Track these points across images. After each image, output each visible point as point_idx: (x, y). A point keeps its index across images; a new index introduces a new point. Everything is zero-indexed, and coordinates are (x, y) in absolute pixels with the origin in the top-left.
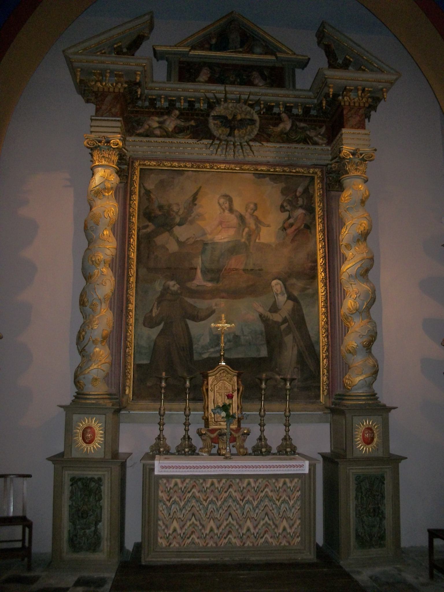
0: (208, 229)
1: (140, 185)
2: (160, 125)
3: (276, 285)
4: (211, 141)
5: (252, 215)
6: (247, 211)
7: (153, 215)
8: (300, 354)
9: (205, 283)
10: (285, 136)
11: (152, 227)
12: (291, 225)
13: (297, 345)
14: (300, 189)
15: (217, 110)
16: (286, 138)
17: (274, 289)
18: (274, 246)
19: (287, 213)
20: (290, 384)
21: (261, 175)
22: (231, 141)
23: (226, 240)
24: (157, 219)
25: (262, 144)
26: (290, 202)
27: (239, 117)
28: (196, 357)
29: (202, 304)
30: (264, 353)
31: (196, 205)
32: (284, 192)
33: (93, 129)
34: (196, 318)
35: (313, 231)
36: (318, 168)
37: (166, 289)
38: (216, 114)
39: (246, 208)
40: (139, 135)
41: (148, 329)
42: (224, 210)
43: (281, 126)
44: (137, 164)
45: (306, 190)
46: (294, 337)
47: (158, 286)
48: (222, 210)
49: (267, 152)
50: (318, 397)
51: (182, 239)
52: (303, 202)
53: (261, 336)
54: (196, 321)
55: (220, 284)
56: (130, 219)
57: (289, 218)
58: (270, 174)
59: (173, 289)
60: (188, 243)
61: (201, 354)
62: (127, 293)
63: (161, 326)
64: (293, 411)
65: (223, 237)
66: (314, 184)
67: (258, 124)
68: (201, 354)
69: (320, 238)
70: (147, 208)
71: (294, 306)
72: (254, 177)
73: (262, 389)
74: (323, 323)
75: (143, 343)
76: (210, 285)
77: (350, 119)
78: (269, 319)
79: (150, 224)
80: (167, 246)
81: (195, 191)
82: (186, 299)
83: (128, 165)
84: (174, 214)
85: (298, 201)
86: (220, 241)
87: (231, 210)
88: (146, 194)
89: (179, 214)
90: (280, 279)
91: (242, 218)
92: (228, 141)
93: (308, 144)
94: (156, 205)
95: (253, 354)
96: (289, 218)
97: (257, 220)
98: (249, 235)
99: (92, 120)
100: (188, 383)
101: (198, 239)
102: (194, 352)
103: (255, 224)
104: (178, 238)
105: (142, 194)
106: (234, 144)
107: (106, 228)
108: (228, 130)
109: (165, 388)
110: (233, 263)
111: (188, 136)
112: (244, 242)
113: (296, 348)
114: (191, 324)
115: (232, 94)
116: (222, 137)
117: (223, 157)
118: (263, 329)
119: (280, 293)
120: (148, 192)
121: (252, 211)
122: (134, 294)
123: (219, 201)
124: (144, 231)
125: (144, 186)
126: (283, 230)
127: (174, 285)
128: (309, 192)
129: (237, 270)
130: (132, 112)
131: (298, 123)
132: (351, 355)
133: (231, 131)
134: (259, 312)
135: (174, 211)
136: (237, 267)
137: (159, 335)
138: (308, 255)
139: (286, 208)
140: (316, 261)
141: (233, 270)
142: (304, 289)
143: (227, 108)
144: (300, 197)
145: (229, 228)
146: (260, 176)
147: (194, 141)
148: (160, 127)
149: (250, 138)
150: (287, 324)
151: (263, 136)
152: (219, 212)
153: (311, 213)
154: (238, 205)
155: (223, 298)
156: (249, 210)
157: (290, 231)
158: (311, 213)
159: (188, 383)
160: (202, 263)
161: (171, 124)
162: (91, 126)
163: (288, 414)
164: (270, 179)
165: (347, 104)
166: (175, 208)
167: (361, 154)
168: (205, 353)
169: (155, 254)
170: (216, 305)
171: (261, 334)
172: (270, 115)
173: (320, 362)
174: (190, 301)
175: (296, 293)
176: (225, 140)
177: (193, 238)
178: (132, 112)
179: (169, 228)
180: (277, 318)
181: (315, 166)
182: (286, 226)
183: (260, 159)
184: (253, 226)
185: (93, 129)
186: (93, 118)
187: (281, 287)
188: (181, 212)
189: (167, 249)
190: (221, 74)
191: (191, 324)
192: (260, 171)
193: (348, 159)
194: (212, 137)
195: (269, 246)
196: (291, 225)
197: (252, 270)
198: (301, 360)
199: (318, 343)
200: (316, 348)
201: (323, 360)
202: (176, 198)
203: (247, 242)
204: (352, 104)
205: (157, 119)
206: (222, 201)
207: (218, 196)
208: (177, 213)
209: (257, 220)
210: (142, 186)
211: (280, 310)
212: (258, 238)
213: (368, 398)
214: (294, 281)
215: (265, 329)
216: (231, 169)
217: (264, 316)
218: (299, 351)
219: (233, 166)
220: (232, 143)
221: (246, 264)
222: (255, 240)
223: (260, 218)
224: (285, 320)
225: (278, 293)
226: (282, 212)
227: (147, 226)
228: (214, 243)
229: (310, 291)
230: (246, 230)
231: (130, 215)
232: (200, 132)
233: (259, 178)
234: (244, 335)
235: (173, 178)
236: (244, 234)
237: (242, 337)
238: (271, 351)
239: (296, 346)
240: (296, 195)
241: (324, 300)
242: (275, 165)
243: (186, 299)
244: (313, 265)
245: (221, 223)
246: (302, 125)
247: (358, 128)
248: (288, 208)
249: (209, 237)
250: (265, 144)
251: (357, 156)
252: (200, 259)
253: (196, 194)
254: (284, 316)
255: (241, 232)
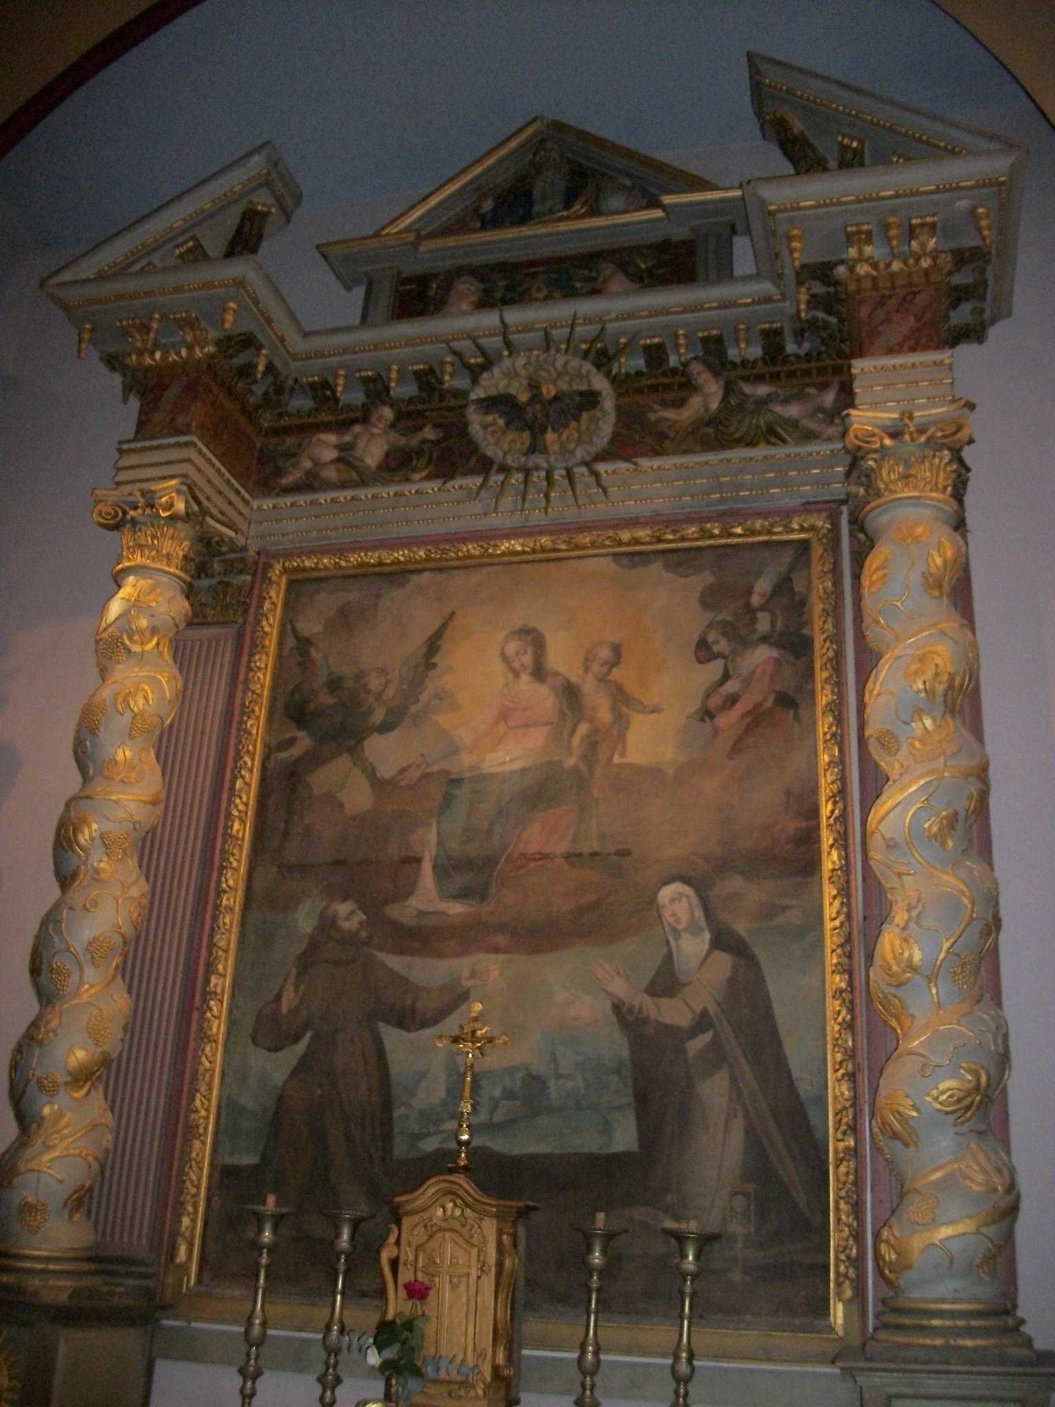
0: (465, 736)
1: (283, 626)
2: (343, 454)
3: (672, 900)
4: (478, 480)
5: (603, 680)
6: (587, 669)
7: (312, 707)
8: (755, 1145)
9: (441, 906)
10: (711, 430)
11: (305, 742)
12: (732, 700)
13: (746, 1112)
14: (763, 586)
15: (483, 383)
16: (715, 434)
17: (667, 916)
18: (671, 772)
19: (720, 663)
20: (697, 1257)
21: (637, 559)
22: (538, 468)
23: (516, 766)
24: (323, 717)
25: (635, 464)
26: (729, 630)
27: (548, 391)
28: (400, 1148)
29: (427, 972)
30: (625, 1138)
31: (434, 666)
32: (709, 600)
33: (121, 477)
34: (407, 1019)
35: (804, 714)
36: (820, 511)
37: (327, 925)
38: (483, 395)
39: (587, 660)
40: (288, 490)
41: (263, 1051)
42: (516, 674)
43: (695, 402)
44: (278, 568)
45: (783, 586)
46: (733, 1080)
47: (304, 920)
48: (511, 676)
49: (653, 486)
50: (821, 1308)
51: (385, 772)
52: (773, 623)
53: (614, 1078)
54: (408, 1030)
55: (486, 908)
56: (241, 722)
57: (726, 677)
58: (663, 552)
59: (346, 925)
60: (403, 784)
61: (416, 1137)
62: (211, 944)
63: (302, 1046)
64: (609, 1351)
65: (509, 757)
66: (808, 565)
67: (609, 404)
68: (416, 1137)
69: (825, 734)
70: (298, 686)
71: (735, 968)
72: (613, 566)
73: (590, 1270)
74: (837, 1028)
75: (248, 1101)
76: (457, 909)
77: (880, 328)
78: (646, 1020)
79: (301, 734)
80: (342, 796)
81: (436, 625)
82: (383, 957)
83: (254, 574)
84: (371, 699)
85: (754, 620)
86: (500, 770)
87: (539, 673)
88: (299, 650)
89: (385, 697)
90: (686, 881)
91: (571, 694)
92: (527, 472)
93: (784, 441)
94: (321, 680)
95: (589, 1142)
96: (726, 677)
97: (621, 698)
98: (592, 744)
99: (121, 451)
100: (345, 1235)
101: (434, 769)
102: (397, 1130)
103: (614, 708)
104: (374, 769)
105: (285, 652)
106: (549, 477)
107: (123, 743)
108: (526, 435)
109: (272, 1250)
110: (534, 836)
111: (424, 474)
112: (576, 769)
113: (739, 1124)
114: (391, 1036)
115: (530, 331)
116: (509, 460)
117: (516, 521)
118: (625, 1053)
119: (685, 930)
120: (304, 644)
121: (605, 669)
122: (233, 946)
123: (503, 648)
124: (284, 755)
125: (294, 630)
126: (702, 720)
127: (352, 913)
128: (792, 590)
129: (545, 856)
130: (275, 432)
131: (747, 389)
132: (898, 1144)
133: (533, 436)
134: (611, 995)
135: (370, 692)
136: (547, 849)
137: (294, 1073)
138: (789, 793)
139: (716, 648)
140: (815, 813)
141: (532, 858)
142: (770, 911)
143: (512, 375)
144: (762, 608)
145: (526, 726)
146: (635, 559)
147: (436, 485)
148: (340, 460)
149: (594, 450)
150: (707, 1037)
151: (637, 437)
152: (501, 680)
153: (797, 657)
154: (562, 656)
155: (496, 950)
156: (595, 668)
157: (728, 719)
158: (797, 657)
159: (345, 1235)
160: (440, 843)
161: (373, 452)
162: (119, 469)
163: (683, 1368)
164: (667, 566)
165: (867, 284)
166: (374, 683)
167: (922, 430)
168: (429, 1134)
169: (306, 821)
170: (473, 974)
171: (618, 1071)
172: (659, 379)
173: (826, 1173)
174: (395, 962)
175: (741, 927)
176: (519, 469)
177: (418, 766)
178: (275, 432)
179: (352, 743)
180: (673, 1013)
181: (808, 507)
182: (714, 702)
183: (632, 508)
184: (604, 715)
185: (121, 477)
186: (125, 447)
187: (691, 908)
188: (391, 691)
189: (341, 805)
190: (506, 283)
191: (391, 1036)
192: (628, 544)
193: (875, 451)
194: (485, 466)
195: (653, 772)
196: (732, 700)
197: (594, 855)
198: (758, 1166)
199: (821, 1100)
200: (815, 1121)
201: (837, 1166)
202: (380, 654)
203: (583, 767)
204: (883, 283)
205: (331, 438)
206: (512, 647)
207: (501, 635)
208: (379, 696)
209: (621, 698)
210: (289, 627)
211: (685, 985)
212: (620, 748)
213: (961, 1323)
214: (735, 883)
215: (632, 1053)
216: (543, 550)
217: (631, 1010)
218: (749, 1131)
219: (545, 541)
220: (543, 474)
221: (575, 841)
222: (611, 759)
223: (631, 688)
224: (703, 1022)
225: (680, 927)
226: (700, 662)
227: (292, 742)
228: (482, 778)
229: (793, 917)
230: (583, 728)
231: (243, 713)
232: (454, 456)
233: (632, 566)
234: (559, 1077)
235: (378, 596)
236: (576, 741)
237: (552, 1083)
238: (649, 1130)
239: (740, 1114)
240: (748, 604)
241: (841, 946)
242: (677, 522)
243: (383, 957)
244: (804, 824)
245: (504, 716)
246: (763, 390)
247: (913, 349)
248: (722, 646)
249: (467, 759)
250: (645, 463)
251: (907, 437)
252: (434, 830)
253: (440, 633)
254: (698, 1009)
255: (566, 735)
